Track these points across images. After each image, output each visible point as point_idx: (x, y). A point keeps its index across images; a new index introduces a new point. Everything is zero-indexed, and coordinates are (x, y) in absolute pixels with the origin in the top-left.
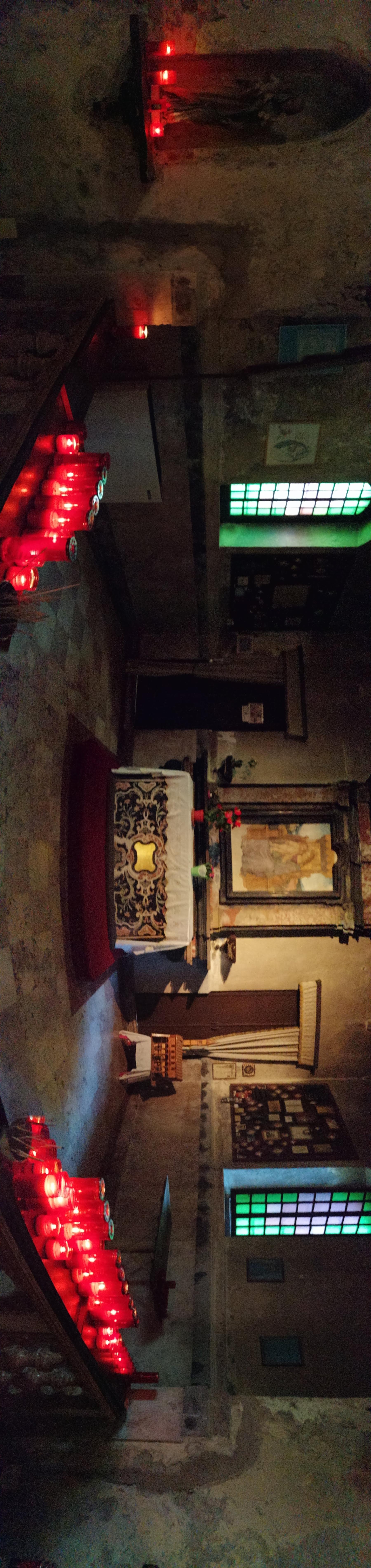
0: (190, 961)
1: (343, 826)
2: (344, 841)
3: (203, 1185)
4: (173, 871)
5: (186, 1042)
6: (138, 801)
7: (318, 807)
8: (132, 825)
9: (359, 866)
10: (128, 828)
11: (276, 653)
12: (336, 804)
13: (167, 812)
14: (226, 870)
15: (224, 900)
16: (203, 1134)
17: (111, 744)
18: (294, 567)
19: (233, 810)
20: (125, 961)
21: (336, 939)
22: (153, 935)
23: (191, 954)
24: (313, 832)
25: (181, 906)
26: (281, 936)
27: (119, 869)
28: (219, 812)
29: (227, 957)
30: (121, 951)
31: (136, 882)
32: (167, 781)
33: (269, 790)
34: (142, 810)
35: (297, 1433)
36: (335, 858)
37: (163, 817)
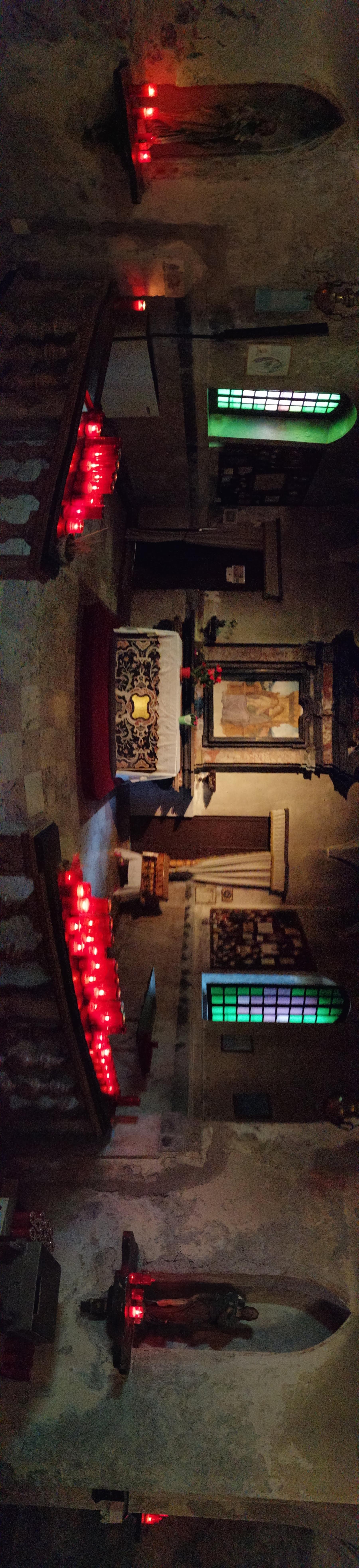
0: (177, 789)
1: (309, 684)
2: (309, 697)
3: (184, 984)
4: (164, 719)
5: (173, 863)
6: (135, 659)
7: (289, 666)
8: (130, 680)
9: (321, 718)
10: (127, 683)
11: (257, 524)
12: (305, 663)
13: (159, 669)
14: (208, 719)
15: (206, 743)
16: (185, 947)
17: (112, 605)
18: (274, 457)
19: (215, 668)
20: (123, 787)
21: (301, 775)
22: (147, 767)
23: (178, 784)
24: (284, 688)
25: (170, 745)
27: (120, 716)
28: (203, 669)
29: (209, 787)
30: (120, 779)
31: (134, 727)
32: (160, 640)
33: (247, 649)
34: (138, 667)
35: (260, 1149)
36: (301, 712)
37: (156, 674)
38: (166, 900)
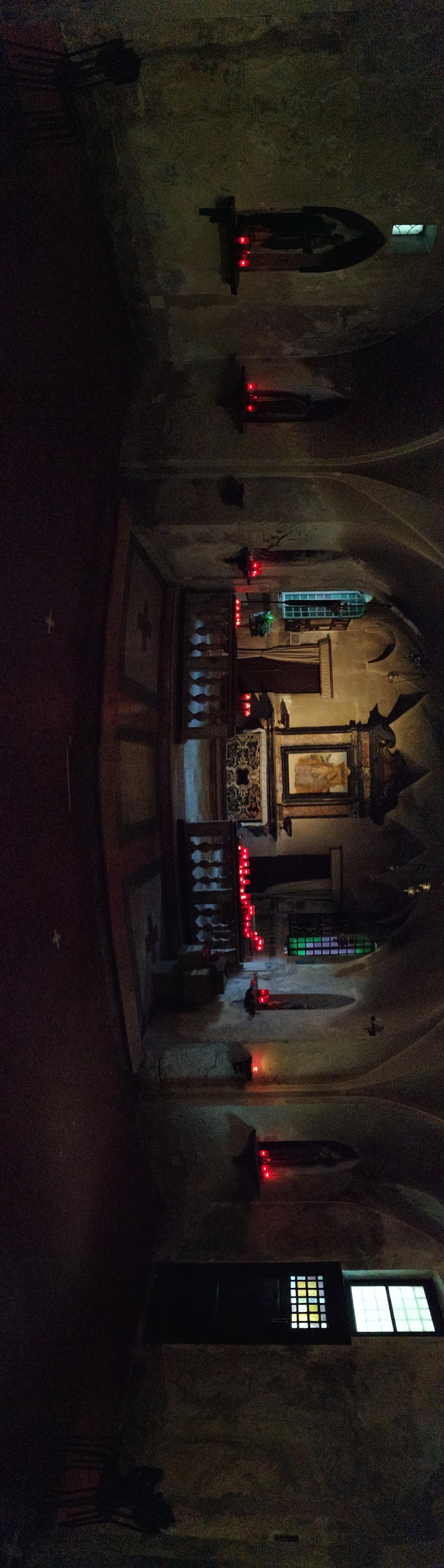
26: (365, 1285)
38: (231, 200)
